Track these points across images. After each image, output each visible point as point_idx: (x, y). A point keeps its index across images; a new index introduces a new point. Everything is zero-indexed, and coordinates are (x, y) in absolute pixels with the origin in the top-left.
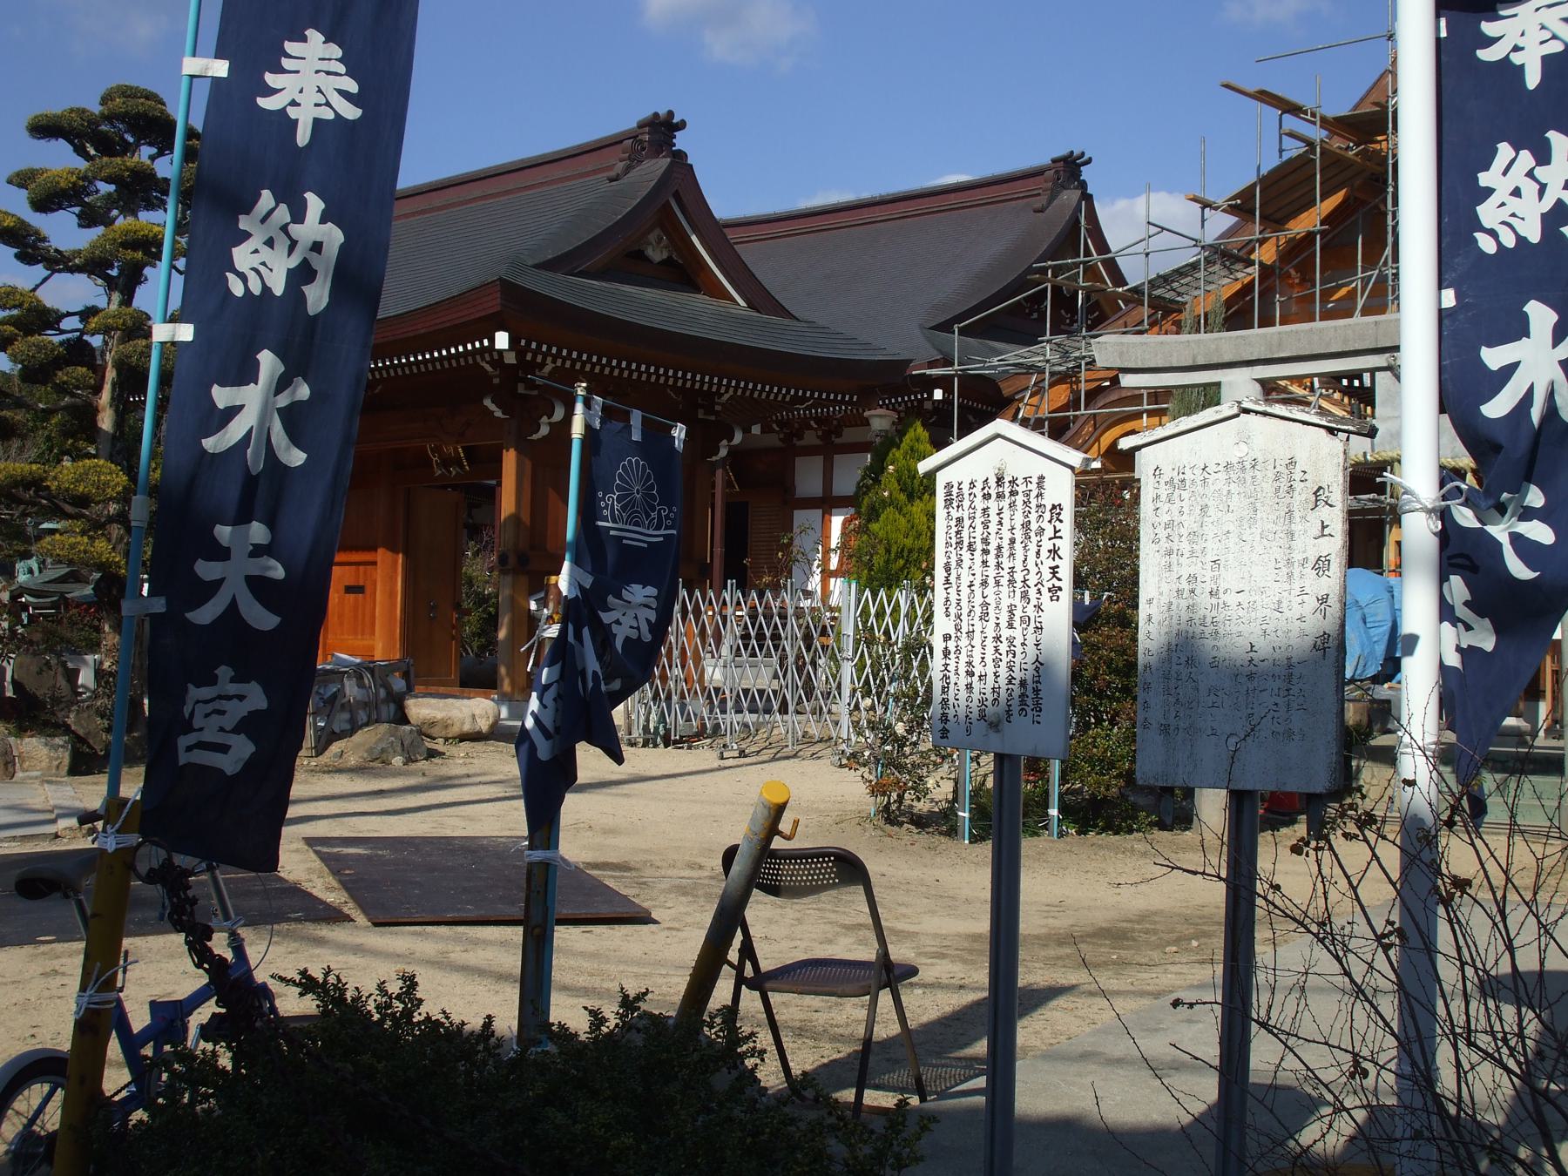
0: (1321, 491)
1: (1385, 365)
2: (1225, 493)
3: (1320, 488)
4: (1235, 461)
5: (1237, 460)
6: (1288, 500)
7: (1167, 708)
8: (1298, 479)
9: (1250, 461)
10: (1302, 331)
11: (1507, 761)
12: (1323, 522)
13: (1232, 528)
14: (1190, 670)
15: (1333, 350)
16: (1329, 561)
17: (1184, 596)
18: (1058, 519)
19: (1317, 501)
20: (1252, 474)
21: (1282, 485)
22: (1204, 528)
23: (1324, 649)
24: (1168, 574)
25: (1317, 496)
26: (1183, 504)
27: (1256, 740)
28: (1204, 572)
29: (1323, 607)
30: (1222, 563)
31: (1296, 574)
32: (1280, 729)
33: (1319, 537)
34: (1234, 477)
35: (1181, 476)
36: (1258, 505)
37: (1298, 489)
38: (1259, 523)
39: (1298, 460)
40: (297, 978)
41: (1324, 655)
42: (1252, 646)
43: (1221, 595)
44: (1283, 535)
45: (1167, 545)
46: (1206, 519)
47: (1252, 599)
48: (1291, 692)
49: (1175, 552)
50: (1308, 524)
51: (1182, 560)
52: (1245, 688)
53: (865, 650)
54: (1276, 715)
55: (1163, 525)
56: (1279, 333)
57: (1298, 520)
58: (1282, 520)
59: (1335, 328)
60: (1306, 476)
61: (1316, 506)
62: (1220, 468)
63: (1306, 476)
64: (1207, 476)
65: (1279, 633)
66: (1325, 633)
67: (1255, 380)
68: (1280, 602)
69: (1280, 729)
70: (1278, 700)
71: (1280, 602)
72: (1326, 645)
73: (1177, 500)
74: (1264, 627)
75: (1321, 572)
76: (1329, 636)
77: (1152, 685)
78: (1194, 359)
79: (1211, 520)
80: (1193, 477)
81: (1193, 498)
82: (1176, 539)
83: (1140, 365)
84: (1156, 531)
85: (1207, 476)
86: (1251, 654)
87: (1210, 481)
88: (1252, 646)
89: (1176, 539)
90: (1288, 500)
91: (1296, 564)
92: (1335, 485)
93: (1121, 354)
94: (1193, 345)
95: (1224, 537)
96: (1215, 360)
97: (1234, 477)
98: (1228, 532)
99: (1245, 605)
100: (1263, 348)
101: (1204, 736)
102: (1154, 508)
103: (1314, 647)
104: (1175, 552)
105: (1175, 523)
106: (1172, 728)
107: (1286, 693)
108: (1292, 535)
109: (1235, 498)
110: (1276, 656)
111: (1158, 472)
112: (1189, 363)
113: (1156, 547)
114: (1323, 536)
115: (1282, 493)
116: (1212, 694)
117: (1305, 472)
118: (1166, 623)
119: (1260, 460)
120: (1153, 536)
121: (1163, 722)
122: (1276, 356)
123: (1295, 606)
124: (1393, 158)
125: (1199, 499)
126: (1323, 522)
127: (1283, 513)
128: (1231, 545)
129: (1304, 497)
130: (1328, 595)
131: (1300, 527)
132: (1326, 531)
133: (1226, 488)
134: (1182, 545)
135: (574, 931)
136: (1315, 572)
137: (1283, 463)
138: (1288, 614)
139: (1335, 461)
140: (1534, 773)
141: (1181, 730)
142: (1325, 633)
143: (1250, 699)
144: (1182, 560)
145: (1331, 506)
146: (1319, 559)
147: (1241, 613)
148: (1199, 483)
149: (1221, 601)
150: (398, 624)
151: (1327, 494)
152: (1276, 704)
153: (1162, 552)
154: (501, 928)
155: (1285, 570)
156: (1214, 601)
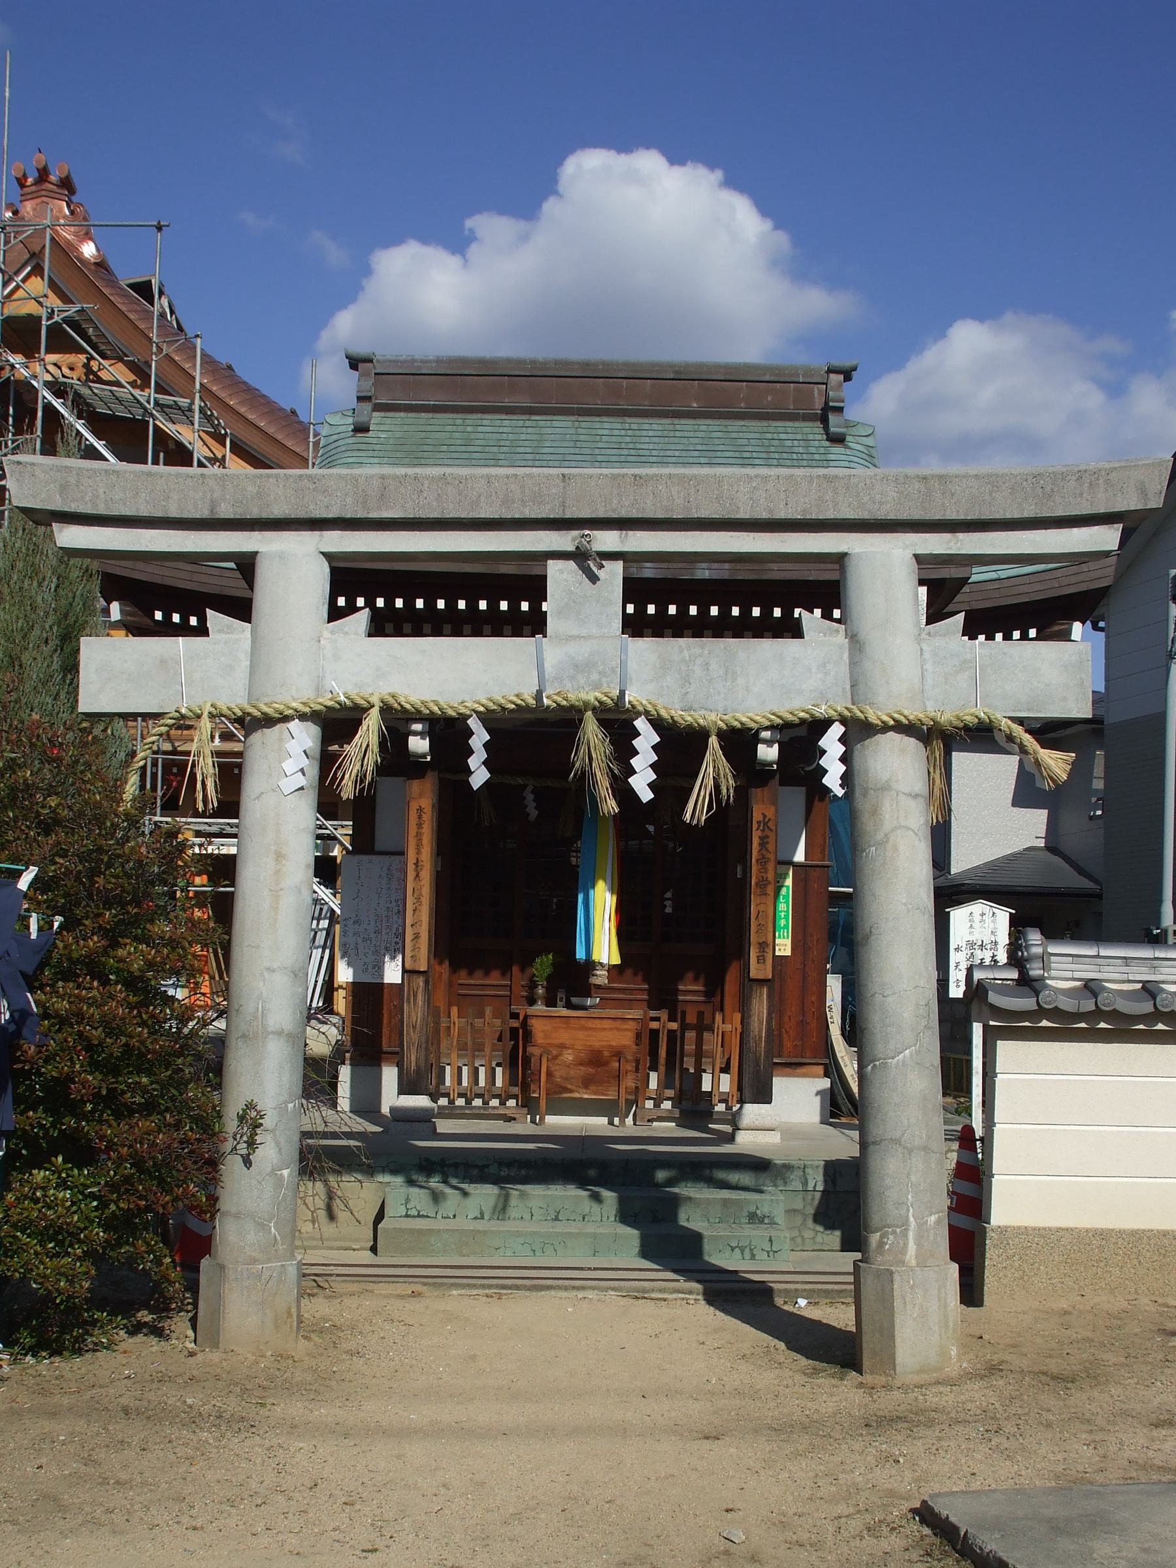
1: (571, 548)
10: (427, 477)
11: (487, 1166)
15: (484, 513)
53: (126, 390)
56: (383, 477)
59: (489, 479)
67: (322, 553)
78: (213, 505)
83: (102, 510)
93: (64, 488)
94: (211, 483)
96: (254, 513)
100: (349, 500)
112: (203, 513)
122: (374, 515)
124: (315, 436)
135: (247, 644)
140: (525, 1181)
154: (1095, 530)
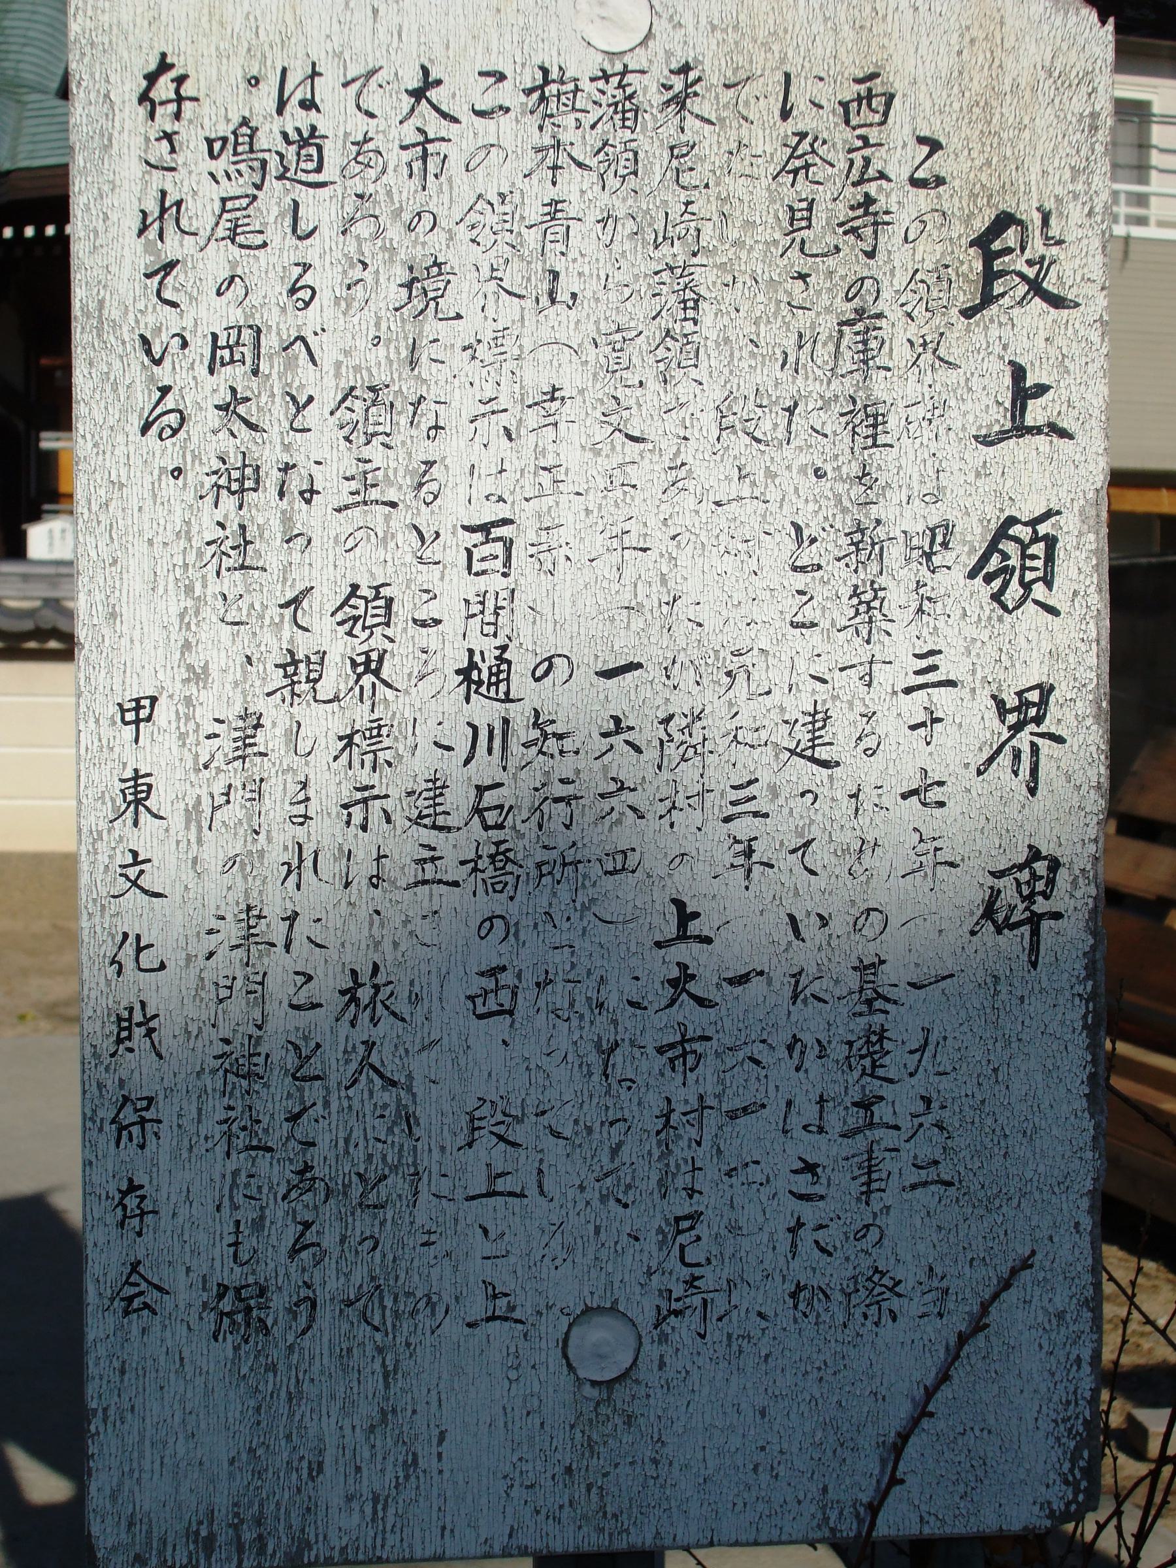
0: (1011, 237)
2: (534, 211)
3: (1004, 221)
4: (581, 66)
5: (593, 63)
6: (849, 264)
7: (247, 1213)
8: (899, 171)
9: (659, 72)
12: (1018, 373)
13: (570, 378)
14: (364, 1029)
16: (1051, 542)
17: (325, 689)
18: (546, 82)
19: (989, 276)
20: (669, 132)
21: (823, 195)
22: (425, 368)
23: (1034, 921)
24: (233, 583)
25: (989, 258)
26: (311, 251)
27: (715, 1332)
28: (429, 576)
29: (1023, 740)
30: (524, 537)
31: (898, 596)
32: (835, 1273)
33: (1003, 436)
34: (582, 145)
35: (297, 119)
36: (705, 278)
37: (903, 219)
38: (712, 359)
39: (899, 86)
40: (424, 101)
41: (1035, 947)
42: (685, 916)
43: (521, 684)
44: (831, 422)
45: (224, 442)
46: (432, 327)
47: (681, 704)
48: (881, 1112)
49: (272, 479)
50: (953, 376)
51: (309, 518)
52: (655, 1103)
54: (810, 1213)
55: (201, 347)
57: (902, 354)
58: (824, 353)
60: (940, 164)
61: (988, 299)
62: (507, 94)
63: (940, 164)
64: (435, 126)
65: (818, 856)
66: (1035, 854)
68: (818, 719)
69: (835, 1273)
70: (820, 1150)
71: (818, 719)
72: (1041, 905)
73: (278, 235)
74: (743, 828)
75: (1014, 591)
76: (1055, 865)
77: (165, 1110)
79: (463, 332)
80: (359, 126)
81: (363, 229)
82: (276, 415)
84: (164, 375)
85: (435, 126)
86: (681, 952)
87: (456, 157)
88: (685, 916)
89: (276, 415)
90: (849, 264)
91: (895, 553)
92: (1076, 213)
95: (533, 418)
97: (582, 145)
98: (553, 394)
99: (648, 733)
101: (452, 1329)
102: (146, 262)
103: (989, 912)
104: (272, 479)
105: (270, 342)
106: (278, 1302)
107: (856, 1118)
108: (876, 421)
109: (586, 237)
110: (805, 956)
111: (164, 88)
113: (169, 453)
114: (1020, 430)
115: (820, 235)
116: (485, 1140)
117: (935, 146)
118: (234, 812)
119: (713, 71)
120: (144, 399)
121: (234, 1276)
123: (890, 726)
125: (395, 233)
126: (1018, 373)
127: (827, 325)
128: (571, 456)
129: (928, 253)
130: (1046, 691)
131: (913, 389)
132: (1036, 413)
133: (538, 192)
134: (307, 449)
136: (983, 590)
137: (827, 95)
138: (867, 772)
139: (1078, 104)
141: (325, 1316)
142: (1035, 854)
143: (680, 1151)
144: (309, 518)
145: (1056, 302)
146: (1002, 533)
147: (624, 764)
148: (396, 158)
149: (519, 715)
150: (1157, 42)
151: (1037, 246)
152: (810, 1168)
153: (197, 475)
155: (841, 578)
156: (485, 711)
